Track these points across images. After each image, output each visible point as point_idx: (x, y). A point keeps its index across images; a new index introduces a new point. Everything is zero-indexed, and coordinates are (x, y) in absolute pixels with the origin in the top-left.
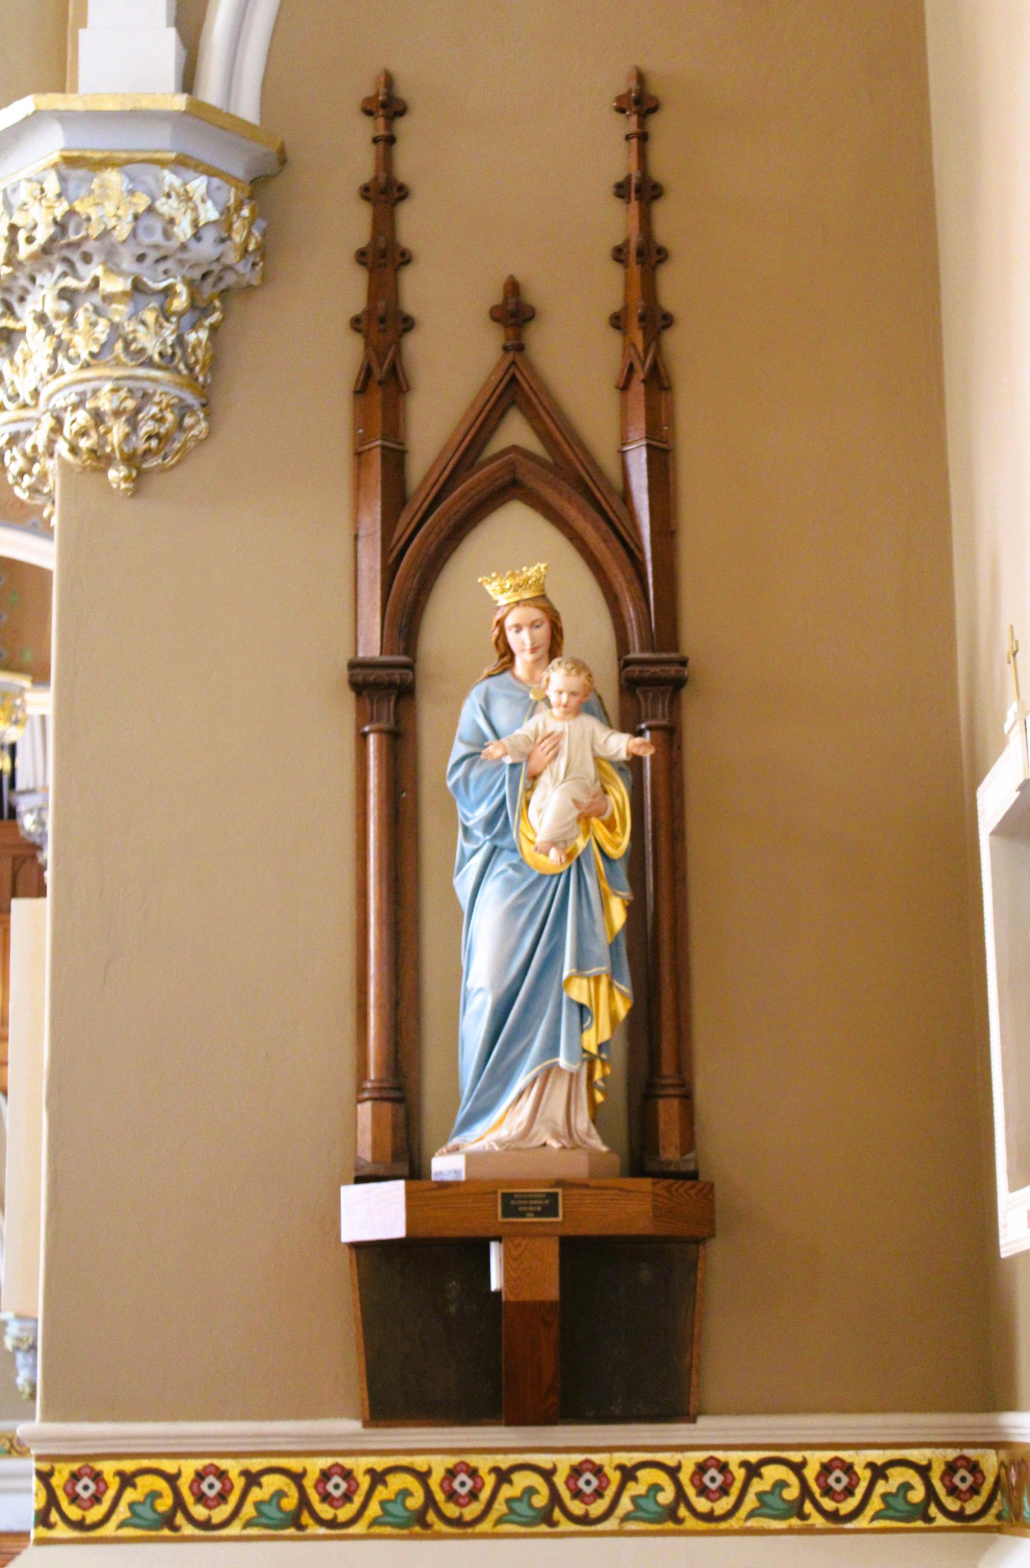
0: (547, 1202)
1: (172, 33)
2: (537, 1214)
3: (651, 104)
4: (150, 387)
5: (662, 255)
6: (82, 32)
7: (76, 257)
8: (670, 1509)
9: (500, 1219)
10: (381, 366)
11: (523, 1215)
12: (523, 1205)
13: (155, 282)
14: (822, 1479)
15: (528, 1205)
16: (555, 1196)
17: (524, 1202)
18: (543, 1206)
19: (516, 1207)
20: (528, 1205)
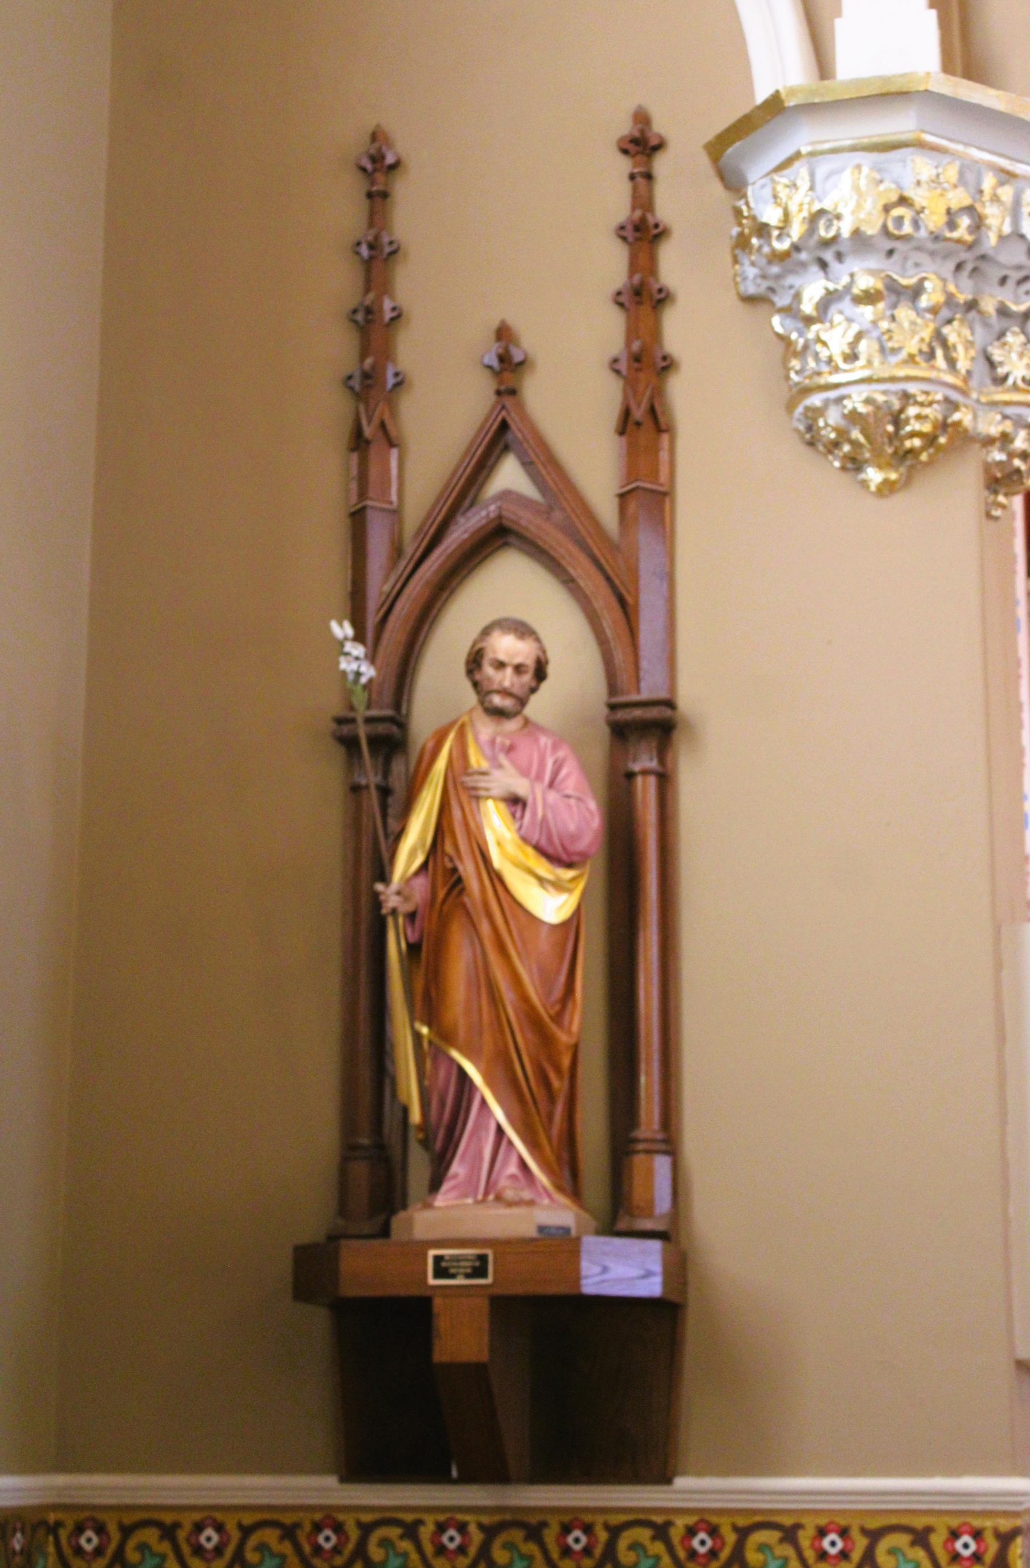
0: (477, 1264)
1: (933, 13)
2: (468, 1276)
3: (654, 142)
4: (912, 388)
5: (662, 299)
6: (838, 22)
7: (828, 256)
8: (825, 1559)
9: (489, 1280)
10: (639, 405)
11: (453, 1276)
12: (454, 1267)
13: (903, 276)
14: (209, 1556)
15: (459, 1267)
16: (483, 1258)
17: (455, 1264)
18: (474, 1268)
19: (446, 1269)
20: (459, 1267)
